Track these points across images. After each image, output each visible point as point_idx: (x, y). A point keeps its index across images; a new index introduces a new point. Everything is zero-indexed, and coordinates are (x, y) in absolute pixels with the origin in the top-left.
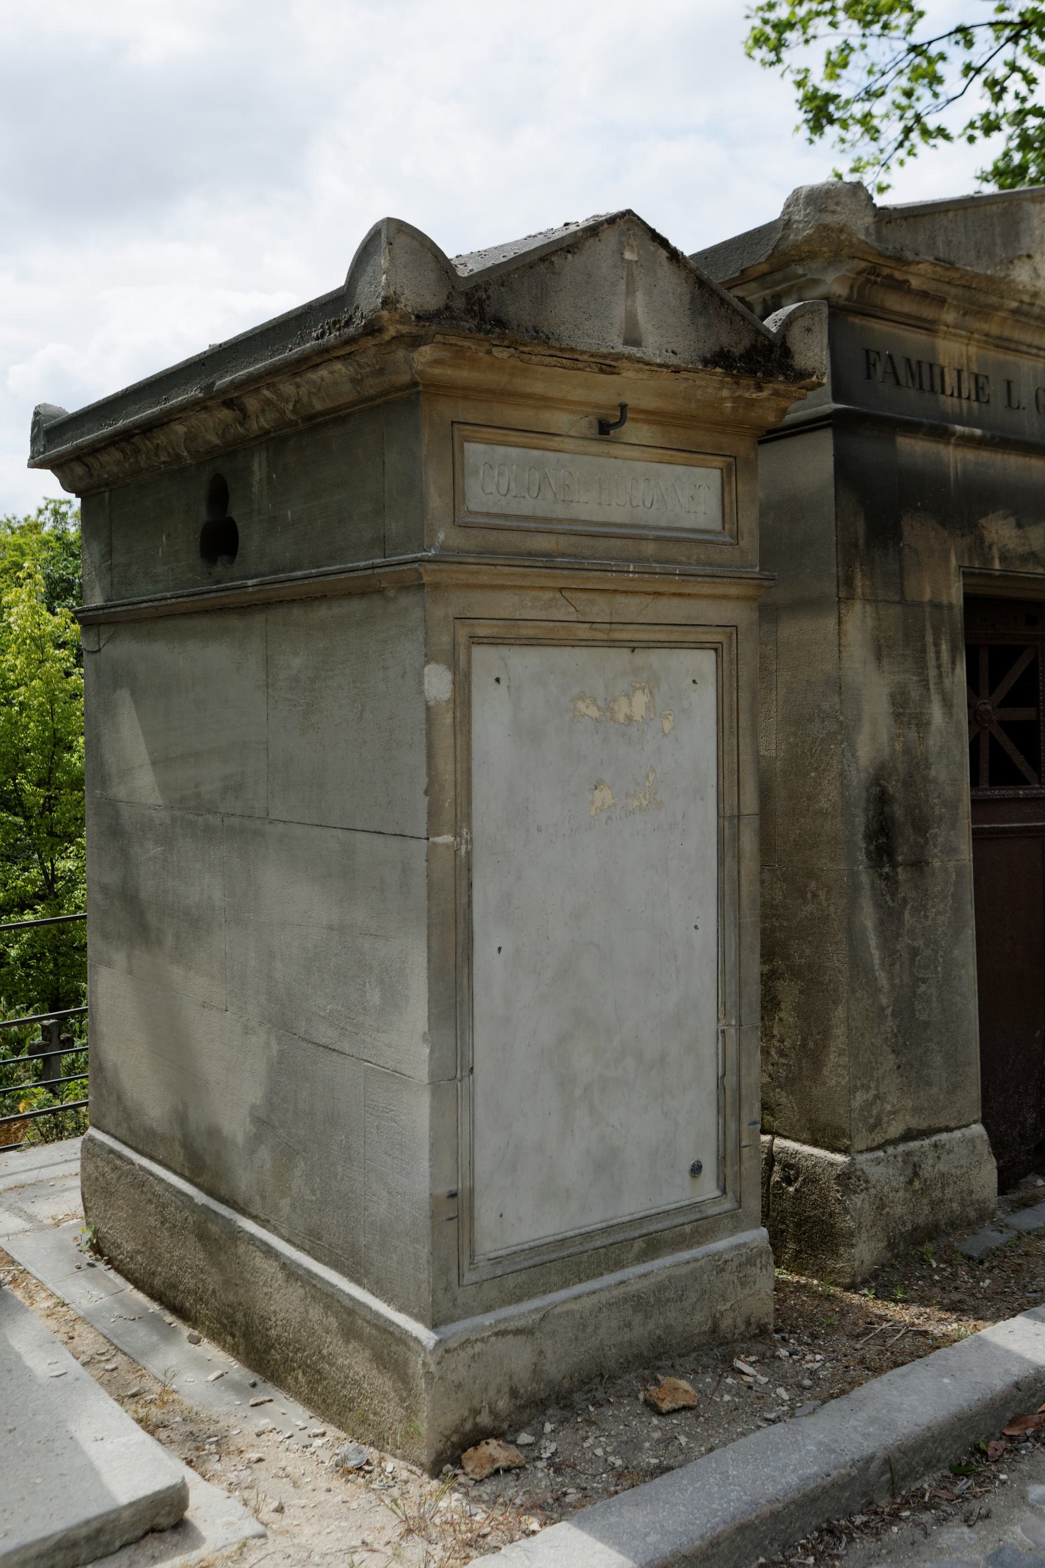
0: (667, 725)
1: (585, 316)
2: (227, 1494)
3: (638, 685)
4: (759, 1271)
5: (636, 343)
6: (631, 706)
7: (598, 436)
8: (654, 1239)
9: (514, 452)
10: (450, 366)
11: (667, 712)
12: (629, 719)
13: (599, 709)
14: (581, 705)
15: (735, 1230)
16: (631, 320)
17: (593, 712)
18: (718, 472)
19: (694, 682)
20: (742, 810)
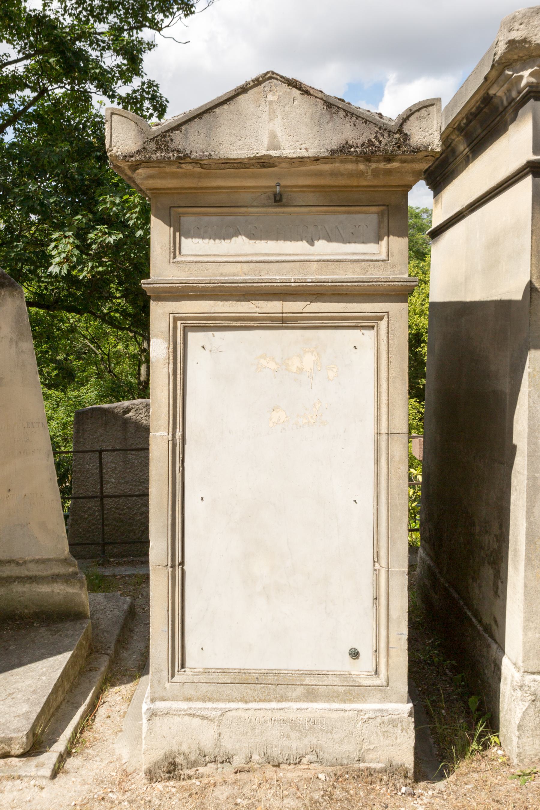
0: (331, 374)
1: (238, 138)
2: (149, 782)
3: (307, 350)
4: (400, 731)
5: (277, 147)
6: (302, 362)
7: (274, 204)
8: (313, 689)
9: (214, 219)
10: (158, 178)
11: (331, 366)
12: (300, 370)
13: (277, 364)
14: (263, 362)
15: (384, 700)
16: (273, 136)
17: (272, 365)
18: (375, 216)
19: (355, 348)
20: (391, 429)
